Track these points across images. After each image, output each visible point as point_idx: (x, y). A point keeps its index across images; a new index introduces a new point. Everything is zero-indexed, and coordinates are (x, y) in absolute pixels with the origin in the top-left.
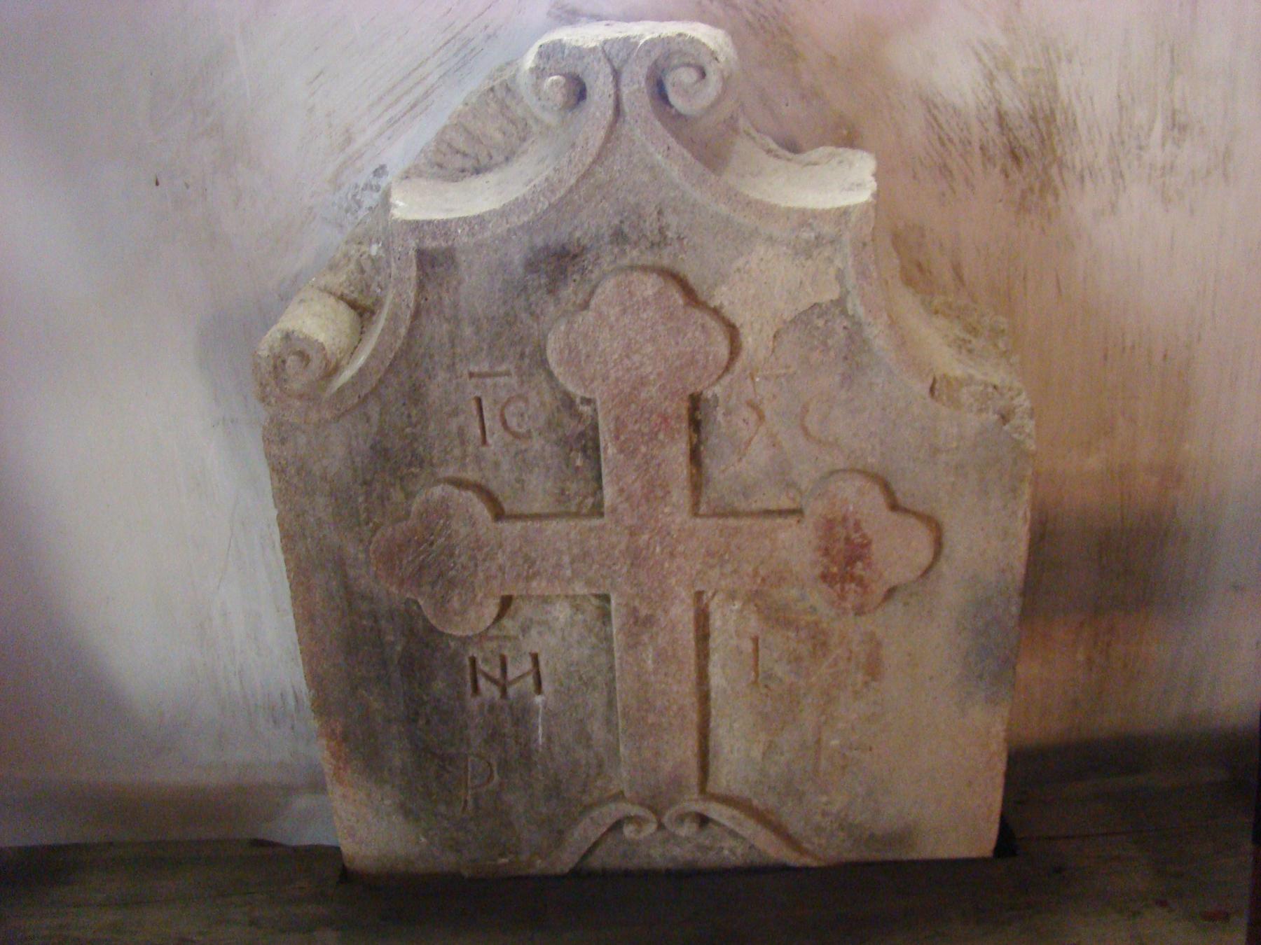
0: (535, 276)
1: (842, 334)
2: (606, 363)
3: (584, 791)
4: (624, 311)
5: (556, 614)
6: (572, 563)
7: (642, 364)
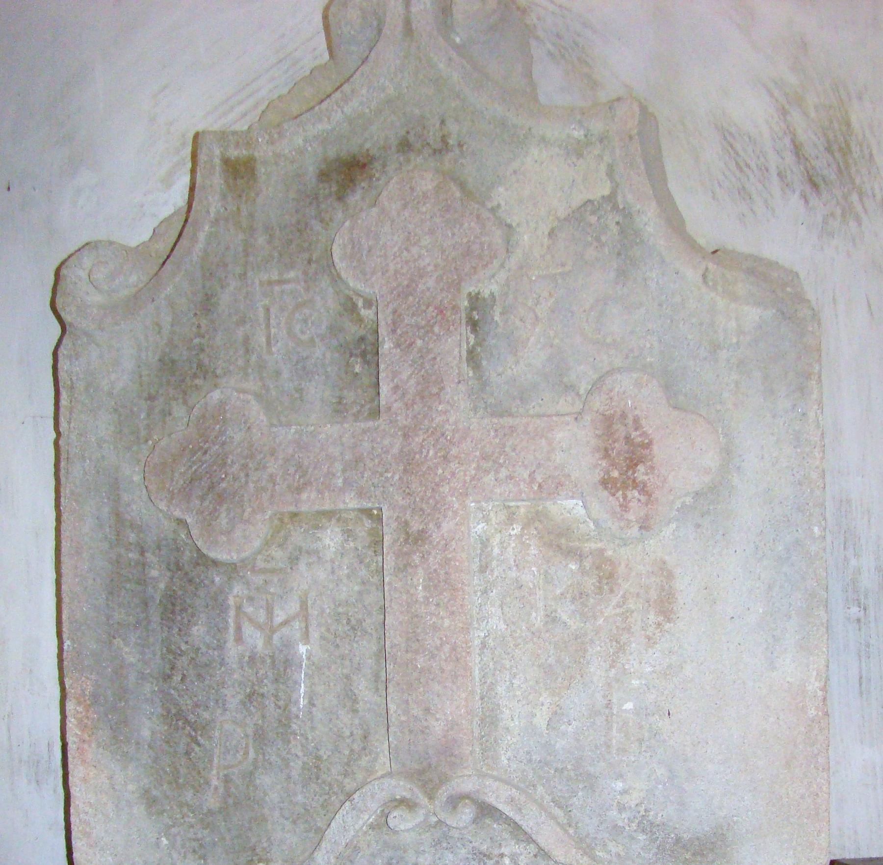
0: (326, 185)
1: (615, 229)
2: (385, 256)
3: (346, 775)
4: (405, 206)
5: (327, 541)
6: (344, 471)
7: (420, 256)
